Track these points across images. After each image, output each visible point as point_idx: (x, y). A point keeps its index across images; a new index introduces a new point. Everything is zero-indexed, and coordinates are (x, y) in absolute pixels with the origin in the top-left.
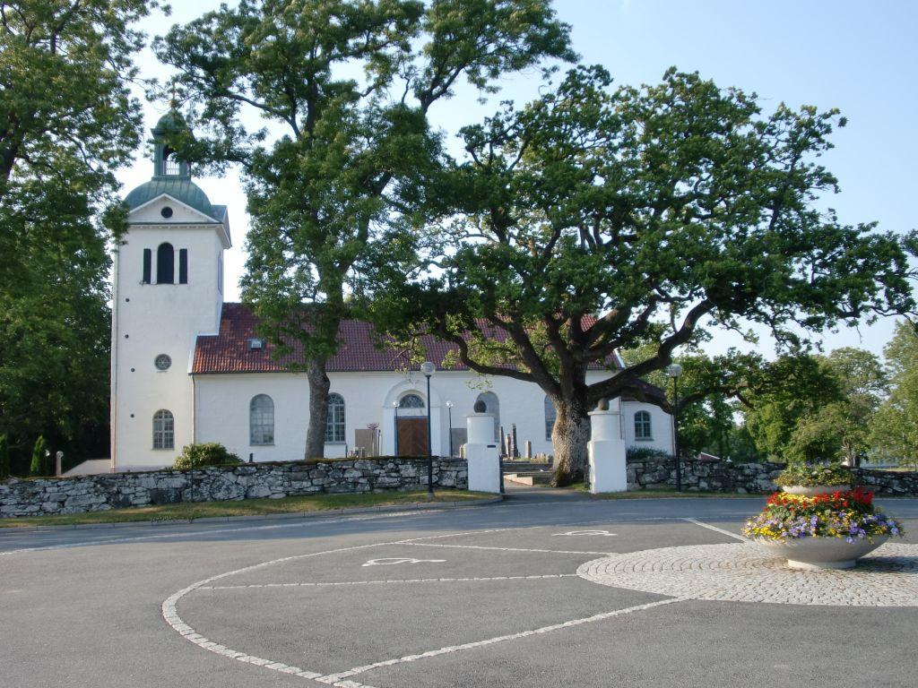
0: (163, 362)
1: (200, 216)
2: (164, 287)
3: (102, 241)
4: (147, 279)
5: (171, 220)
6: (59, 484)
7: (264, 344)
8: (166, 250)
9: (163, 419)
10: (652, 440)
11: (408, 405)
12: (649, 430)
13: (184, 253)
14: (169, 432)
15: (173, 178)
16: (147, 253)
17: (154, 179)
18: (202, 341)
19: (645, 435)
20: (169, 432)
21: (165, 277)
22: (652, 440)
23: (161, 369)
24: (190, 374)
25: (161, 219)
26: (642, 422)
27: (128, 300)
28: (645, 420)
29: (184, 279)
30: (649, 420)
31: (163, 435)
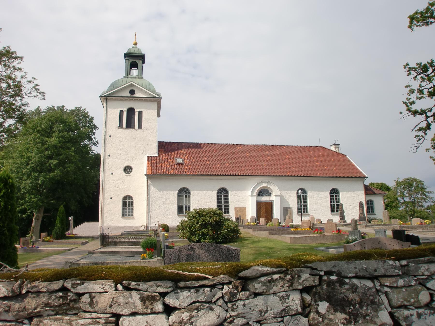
0: (128, 169)
1: (150, 94)
2: (130, 130)
3: (54, 172)
4: (120, 126)
5: (134, 96)
6: (171, 301)
7: (183, 161)
8: (131, 111)
9: (128, 201)
10: (375, 214)
11: (262, 195)
12: (373, 209)
13: (140, 113)
14: (226, 204)
15: (135, 77)
16: (121, 112)
17: (125, 77)
18: (149, 159)
19: (372, 212)
20: (226, 204)
21: (130, 125)
22: (375, 214)
23: (127, 173)
24: (145, 175)
25: (129, 95)
26: (370, 205)
27: (110, 136)
28: (371, 204)
29: (140, 127)
30: (373, 204)
31: (335, 205)
